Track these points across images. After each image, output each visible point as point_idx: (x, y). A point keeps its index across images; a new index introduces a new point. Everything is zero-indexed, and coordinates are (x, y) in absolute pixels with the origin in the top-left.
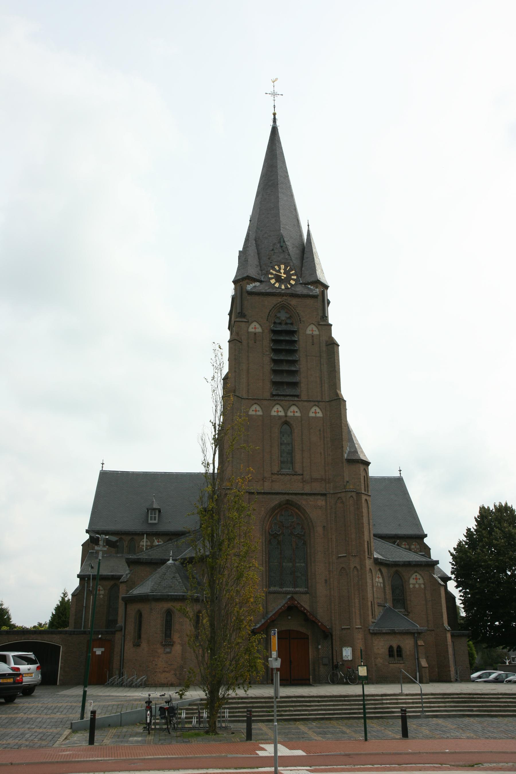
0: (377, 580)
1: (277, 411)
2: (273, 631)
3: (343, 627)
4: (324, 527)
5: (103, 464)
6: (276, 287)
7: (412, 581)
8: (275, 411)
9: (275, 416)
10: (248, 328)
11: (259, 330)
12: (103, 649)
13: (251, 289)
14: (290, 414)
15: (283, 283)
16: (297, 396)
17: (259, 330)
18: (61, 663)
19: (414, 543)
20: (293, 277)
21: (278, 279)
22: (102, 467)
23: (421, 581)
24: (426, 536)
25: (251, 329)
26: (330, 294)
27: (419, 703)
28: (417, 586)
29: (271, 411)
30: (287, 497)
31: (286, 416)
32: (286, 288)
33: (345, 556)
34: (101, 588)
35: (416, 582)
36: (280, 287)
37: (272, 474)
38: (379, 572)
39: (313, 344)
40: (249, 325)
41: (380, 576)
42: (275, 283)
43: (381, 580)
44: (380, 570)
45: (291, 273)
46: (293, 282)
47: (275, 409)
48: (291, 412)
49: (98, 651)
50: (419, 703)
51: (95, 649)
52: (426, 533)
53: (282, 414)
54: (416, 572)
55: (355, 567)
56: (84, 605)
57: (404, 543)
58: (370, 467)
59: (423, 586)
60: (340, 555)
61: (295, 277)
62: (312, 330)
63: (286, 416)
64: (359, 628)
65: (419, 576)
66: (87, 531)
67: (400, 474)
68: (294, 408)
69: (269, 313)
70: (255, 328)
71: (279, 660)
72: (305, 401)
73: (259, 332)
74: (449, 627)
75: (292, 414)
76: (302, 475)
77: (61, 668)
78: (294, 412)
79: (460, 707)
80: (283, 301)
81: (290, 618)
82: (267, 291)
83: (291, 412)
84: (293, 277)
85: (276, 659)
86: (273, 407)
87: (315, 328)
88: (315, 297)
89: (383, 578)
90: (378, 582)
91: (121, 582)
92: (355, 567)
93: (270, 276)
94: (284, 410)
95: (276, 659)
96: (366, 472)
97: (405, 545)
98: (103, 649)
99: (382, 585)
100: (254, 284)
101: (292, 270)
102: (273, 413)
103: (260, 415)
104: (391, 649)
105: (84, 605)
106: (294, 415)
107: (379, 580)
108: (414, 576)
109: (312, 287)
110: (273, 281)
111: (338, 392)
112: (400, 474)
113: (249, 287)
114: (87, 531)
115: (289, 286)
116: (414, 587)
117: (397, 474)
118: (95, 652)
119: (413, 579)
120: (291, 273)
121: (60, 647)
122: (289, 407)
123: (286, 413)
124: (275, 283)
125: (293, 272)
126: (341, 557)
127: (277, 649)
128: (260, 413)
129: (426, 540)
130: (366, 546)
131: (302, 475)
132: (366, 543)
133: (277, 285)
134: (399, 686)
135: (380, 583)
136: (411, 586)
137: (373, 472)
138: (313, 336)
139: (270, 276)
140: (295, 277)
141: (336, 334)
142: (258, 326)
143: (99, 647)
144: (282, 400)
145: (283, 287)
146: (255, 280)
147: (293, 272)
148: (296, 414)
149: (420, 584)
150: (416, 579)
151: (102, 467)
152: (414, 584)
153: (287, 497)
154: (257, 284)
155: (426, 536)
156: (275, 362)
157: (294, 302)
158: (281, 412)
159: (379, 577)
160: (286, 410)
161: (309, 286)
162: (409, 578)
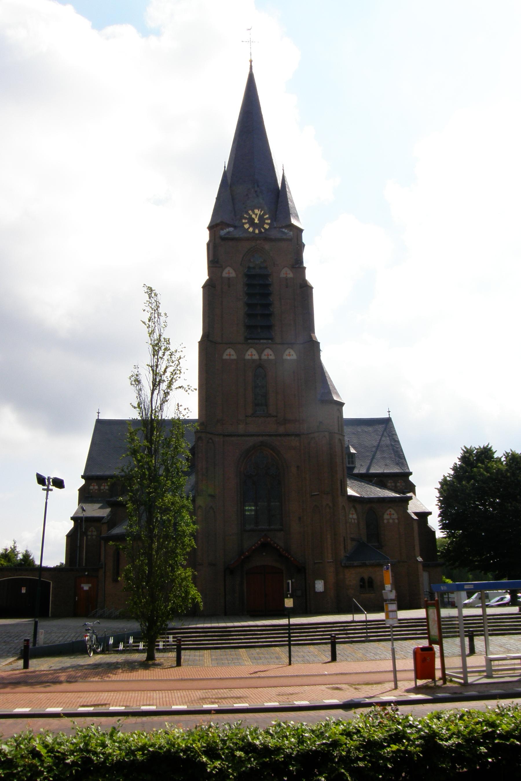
0: (351, 516)
1: (251, 354)
2: (385, 567)
3: (316, 561)
4: (298, 467)
5: (99, 413)
6: (250, 232)
7: (386, 516)
8: (249, 355)
9: (249, 359)
10: (222, 273)
11: (233, 274)
12: (90, 585)
13: (225, 235)
14: (264, 357)
15: (257, 228)
16: (272, 339)
17: (233, 274)
18: (52, 597)
19: (399, 481)
20: (266, 221)
21: (251, 221)
22: (98, 416)
23: (395, 516)
24: (411, 474)
25: (225, 274)
26: (305, 238)
27: (394, 631)
28: (391, 521)
29: (245, 355)
30: (261, 439)
31: (260, 359)
32: (260, 232)
33: (318, 494)
34: (94, 530)
35: (390, 517)
36: (254, 231)
37: (246, 416)
38: (352, 509)
39: (287, 287)
40: (223, 270)
41: (354, 512)
42: (249, 228)
43: (355, 516)
44: (354, 507)
45: (265, 217)
46: (267, 227)
47: (249, 353)
48: (265, 355)
49: (86, 587)
50: (394, 631)
51: (82, 585)
52: (411, 471)
53: (256, 357)
54: (390, 508)
55: (327, 504)
56: (78, 545)
57: (390, 481)
58: (344, 408)
59: (396, 521)
60: (313, 494)
61: (269, 221)
62: (287, 273)
63: (260, 359)
64: (330, 562)
65: (393, 512)
66: (83, 477)
67: (389, 415)
68: (268, 351)
69: (243, 257)
70: (229, 273)
71: (394, 592)
72: (279, 344)
73: (233, 277)
74: (421, 559)
75: (266, 357)
76: (276, 416)
77: (52, 601)
78: (268, 355)
79: (403, 635)
80: (256, 245)
81: (264, 554)
82: (241, 236)
83: (265, 355)
84: (266, 221)
85: (391, 591)
86: (247, 350)
87: (289, 271)
88: (290, 240)
89: (357, 515)
90: (351, 519)
91: (103, 523)
92: (327, 504)
93: (244, 221)
94: (258, 352)
95: (391, 591)
96: (341, 412)
97: (391, 483)
98: (90, 585)
99: (356, 521)
100: (227, 230)
101: (266, 214)
102: (247, 357)
103: (235, 359)
104: (362, 580)
105: (78, 545)
106: (268, 358)
107: (353, 516)
108: (388, 512)
109: (286, 231)
110: (246, 226)
111: (312, 334)
112: (389, 415)
113: (223, 233)
114: (83, 477)
115: (263, 231)
116: (388, 522)
117: (386, 416)
118: (83, 588)
119: (387, 514)
120: (265, 217)
121: (50, 583)
122: (263, 350)
123: (260, 356)
124: (249, 228)
125: (267, 216)
126: (314, 495)
127: (391, 581)
128: (234, 357)
129: (411, 478)
130: (339, 484)
131: (276, 416)
132: (339, 482)
133: (251, 230)
134: (351, 616)
135: (354, 519)
136: (385, 521)
137: (348, 413)
138: (287, 279)
139: (244, 221)
140: (269, 221)
141: (310, 277)
142: (231, 271)
143: (87, 583)
144: (257, 344)
145: (257, 231)
146: (229, 226)
147: (267, 216)
148: (270, 357)
149: (393, 519)
150: (390, 514)
151: (98, 416)
152: (388, 519)
153: (261, 439)
154: (231, 229)
155: (411, 474)
156: (249, 305)
157: (267, 246)
158: (255, 355)
159: (352, 514)
160: (260, 353)
161: (284, 230)
162: (383, 514)
